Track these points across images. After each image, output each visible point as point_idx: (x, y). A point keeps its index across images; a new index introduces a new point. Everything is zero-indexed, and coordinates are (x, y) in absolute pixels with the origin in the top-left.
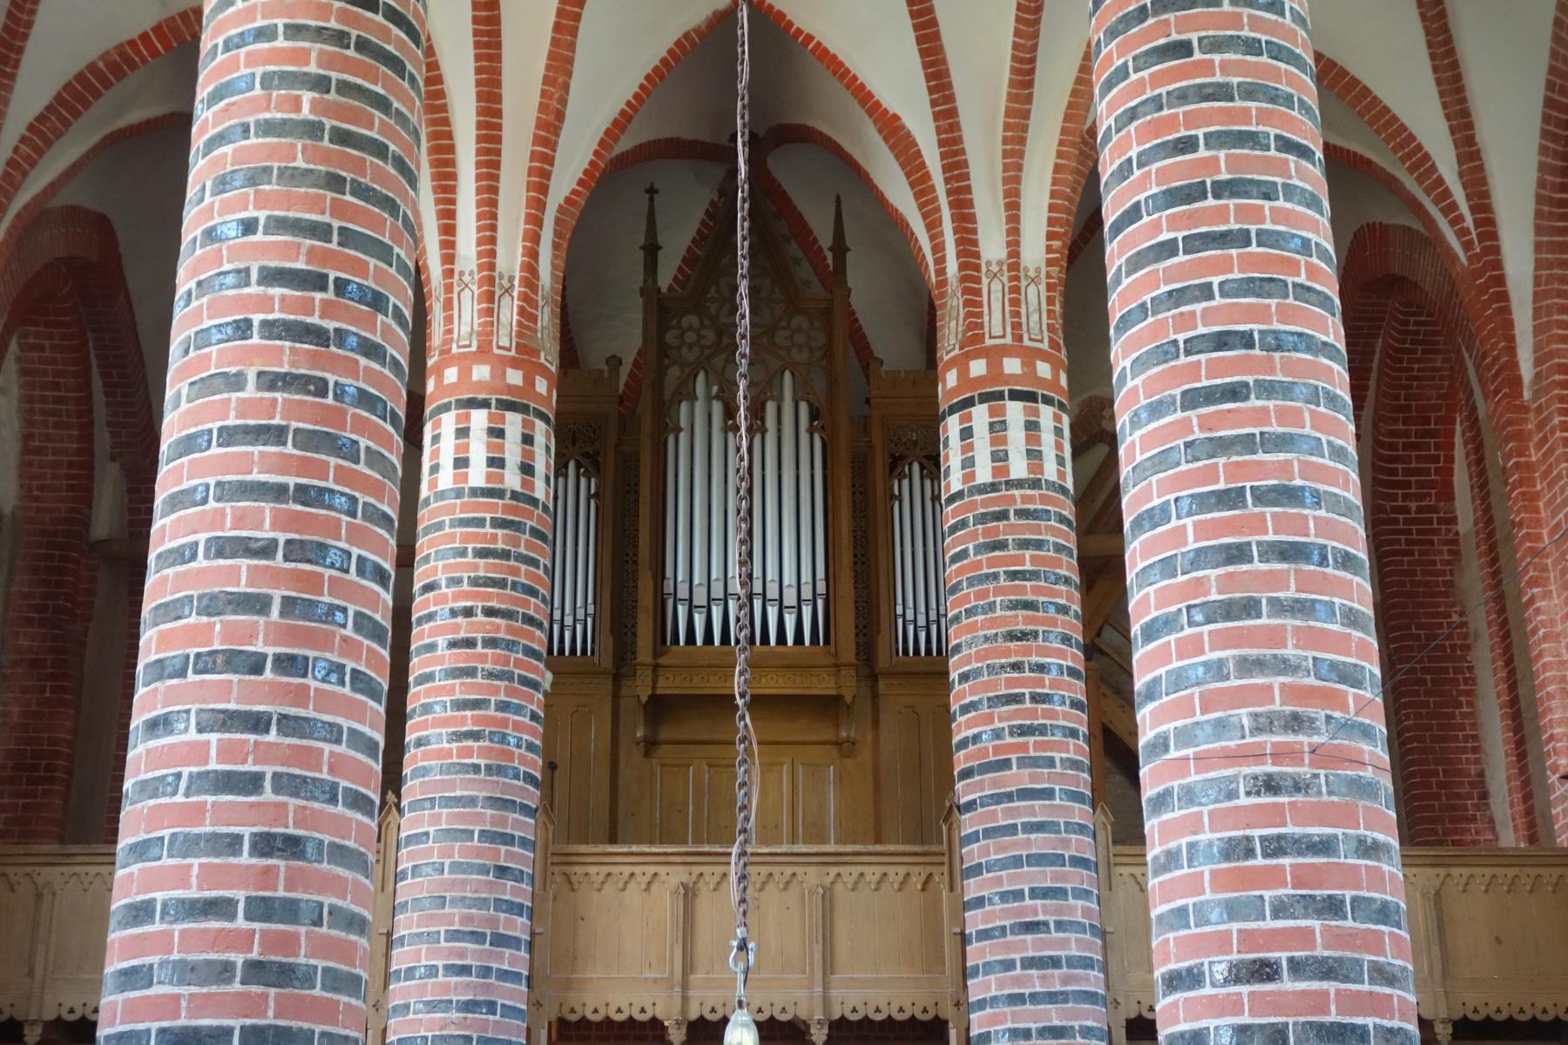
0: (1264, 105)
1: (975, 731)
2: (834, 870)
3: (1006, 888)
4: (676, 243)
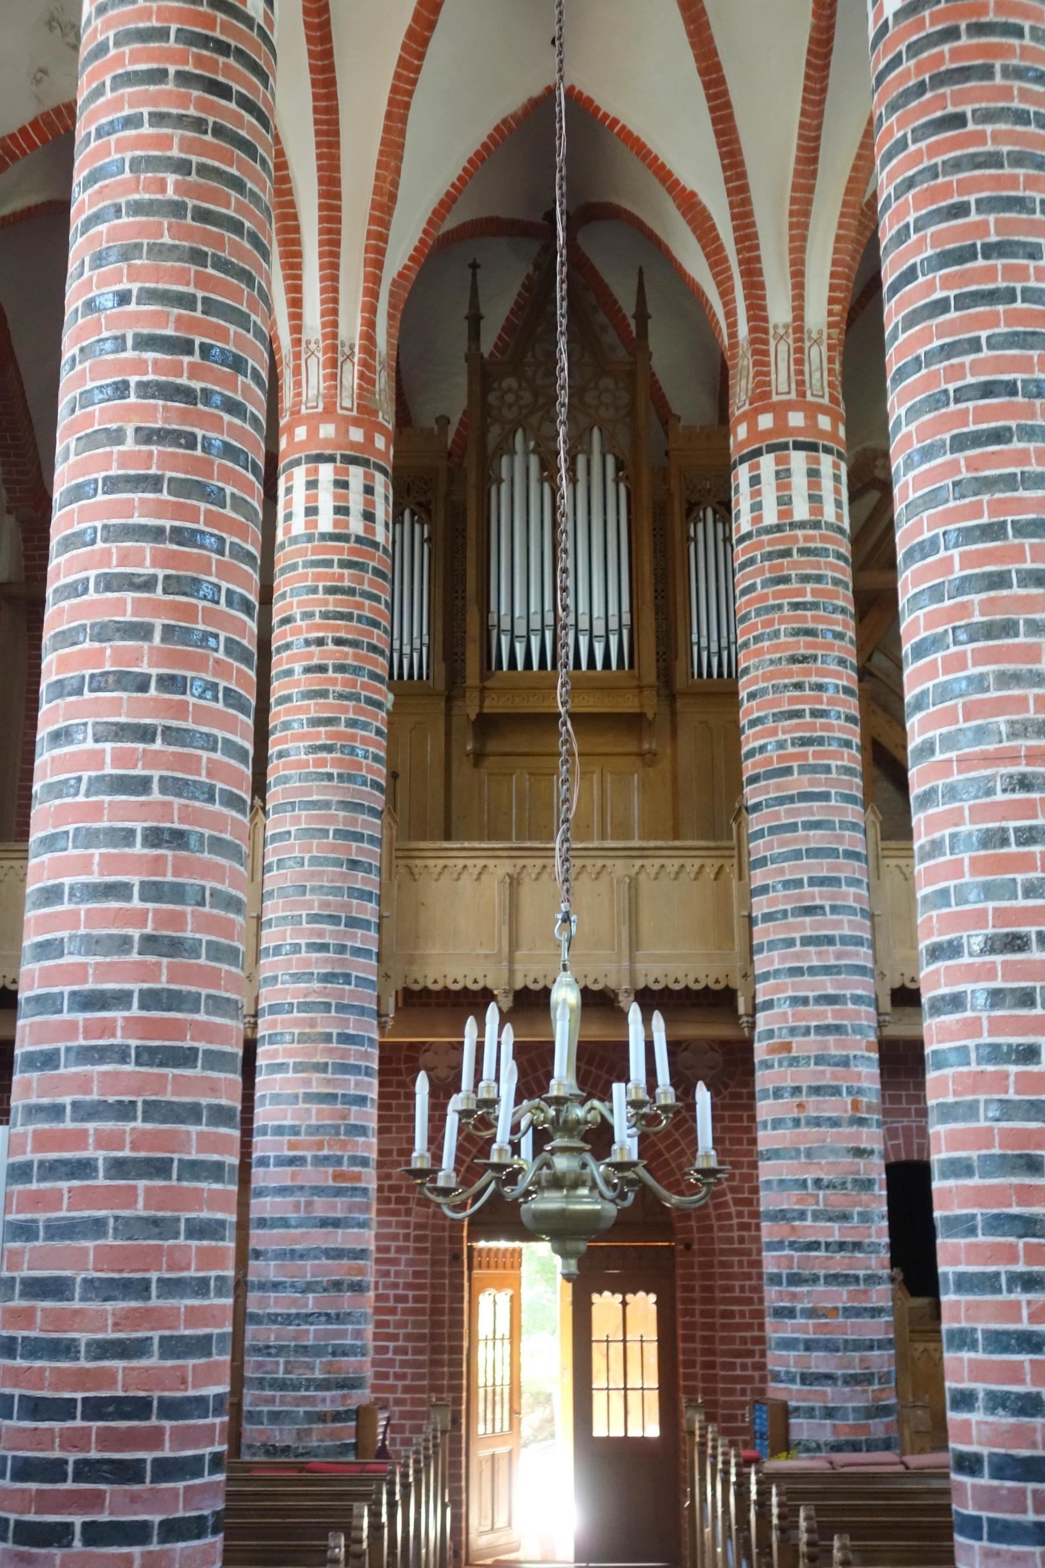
0: (1031, 172)
1: (761, 742)
2: (638, 863)
3: (787, 877)
4: (497, 314)
